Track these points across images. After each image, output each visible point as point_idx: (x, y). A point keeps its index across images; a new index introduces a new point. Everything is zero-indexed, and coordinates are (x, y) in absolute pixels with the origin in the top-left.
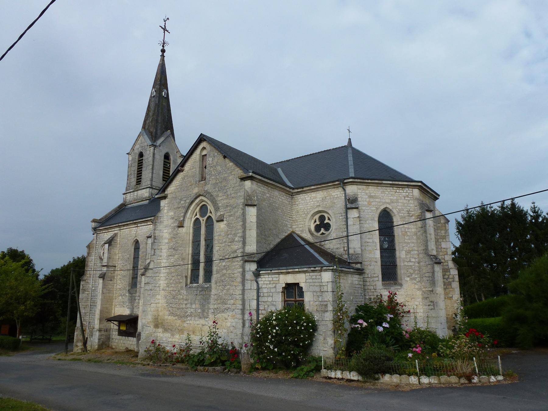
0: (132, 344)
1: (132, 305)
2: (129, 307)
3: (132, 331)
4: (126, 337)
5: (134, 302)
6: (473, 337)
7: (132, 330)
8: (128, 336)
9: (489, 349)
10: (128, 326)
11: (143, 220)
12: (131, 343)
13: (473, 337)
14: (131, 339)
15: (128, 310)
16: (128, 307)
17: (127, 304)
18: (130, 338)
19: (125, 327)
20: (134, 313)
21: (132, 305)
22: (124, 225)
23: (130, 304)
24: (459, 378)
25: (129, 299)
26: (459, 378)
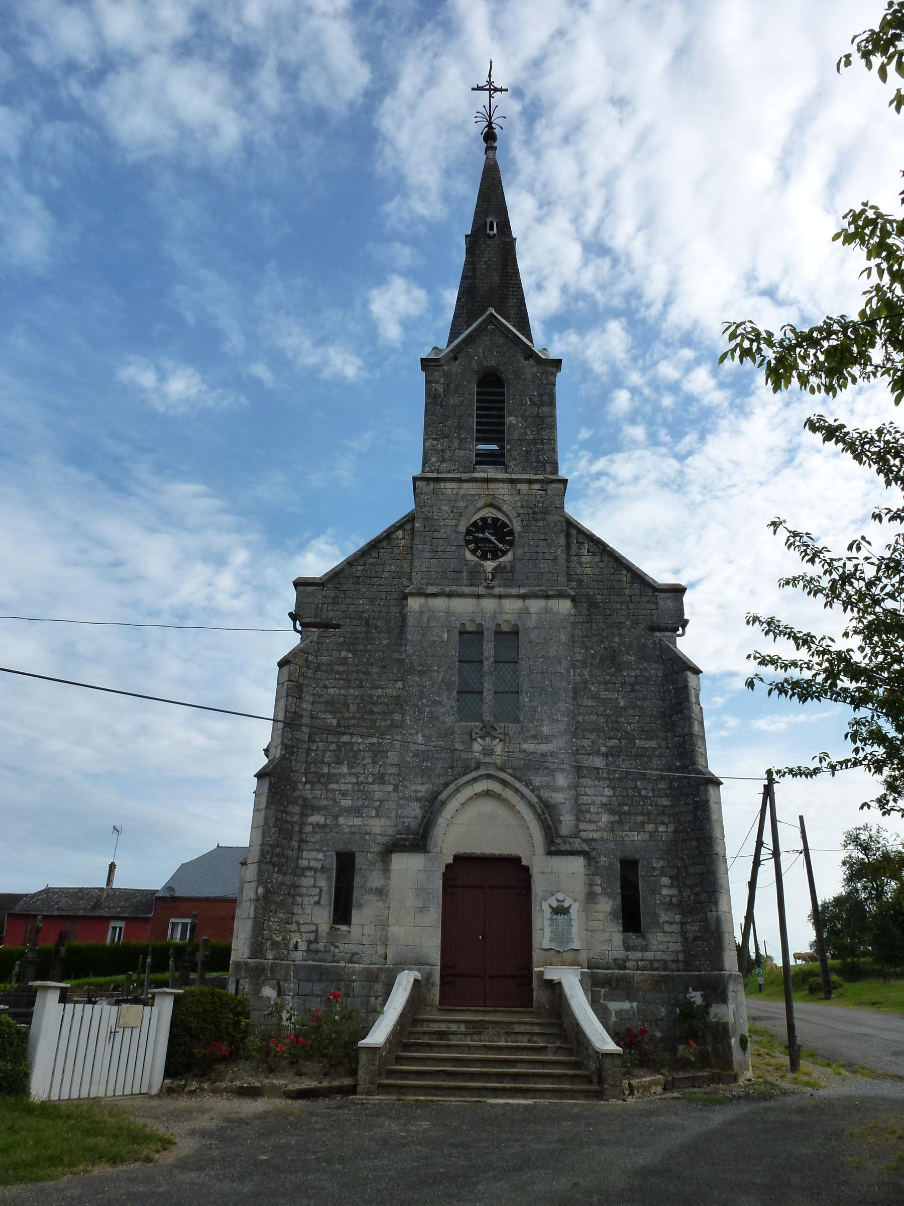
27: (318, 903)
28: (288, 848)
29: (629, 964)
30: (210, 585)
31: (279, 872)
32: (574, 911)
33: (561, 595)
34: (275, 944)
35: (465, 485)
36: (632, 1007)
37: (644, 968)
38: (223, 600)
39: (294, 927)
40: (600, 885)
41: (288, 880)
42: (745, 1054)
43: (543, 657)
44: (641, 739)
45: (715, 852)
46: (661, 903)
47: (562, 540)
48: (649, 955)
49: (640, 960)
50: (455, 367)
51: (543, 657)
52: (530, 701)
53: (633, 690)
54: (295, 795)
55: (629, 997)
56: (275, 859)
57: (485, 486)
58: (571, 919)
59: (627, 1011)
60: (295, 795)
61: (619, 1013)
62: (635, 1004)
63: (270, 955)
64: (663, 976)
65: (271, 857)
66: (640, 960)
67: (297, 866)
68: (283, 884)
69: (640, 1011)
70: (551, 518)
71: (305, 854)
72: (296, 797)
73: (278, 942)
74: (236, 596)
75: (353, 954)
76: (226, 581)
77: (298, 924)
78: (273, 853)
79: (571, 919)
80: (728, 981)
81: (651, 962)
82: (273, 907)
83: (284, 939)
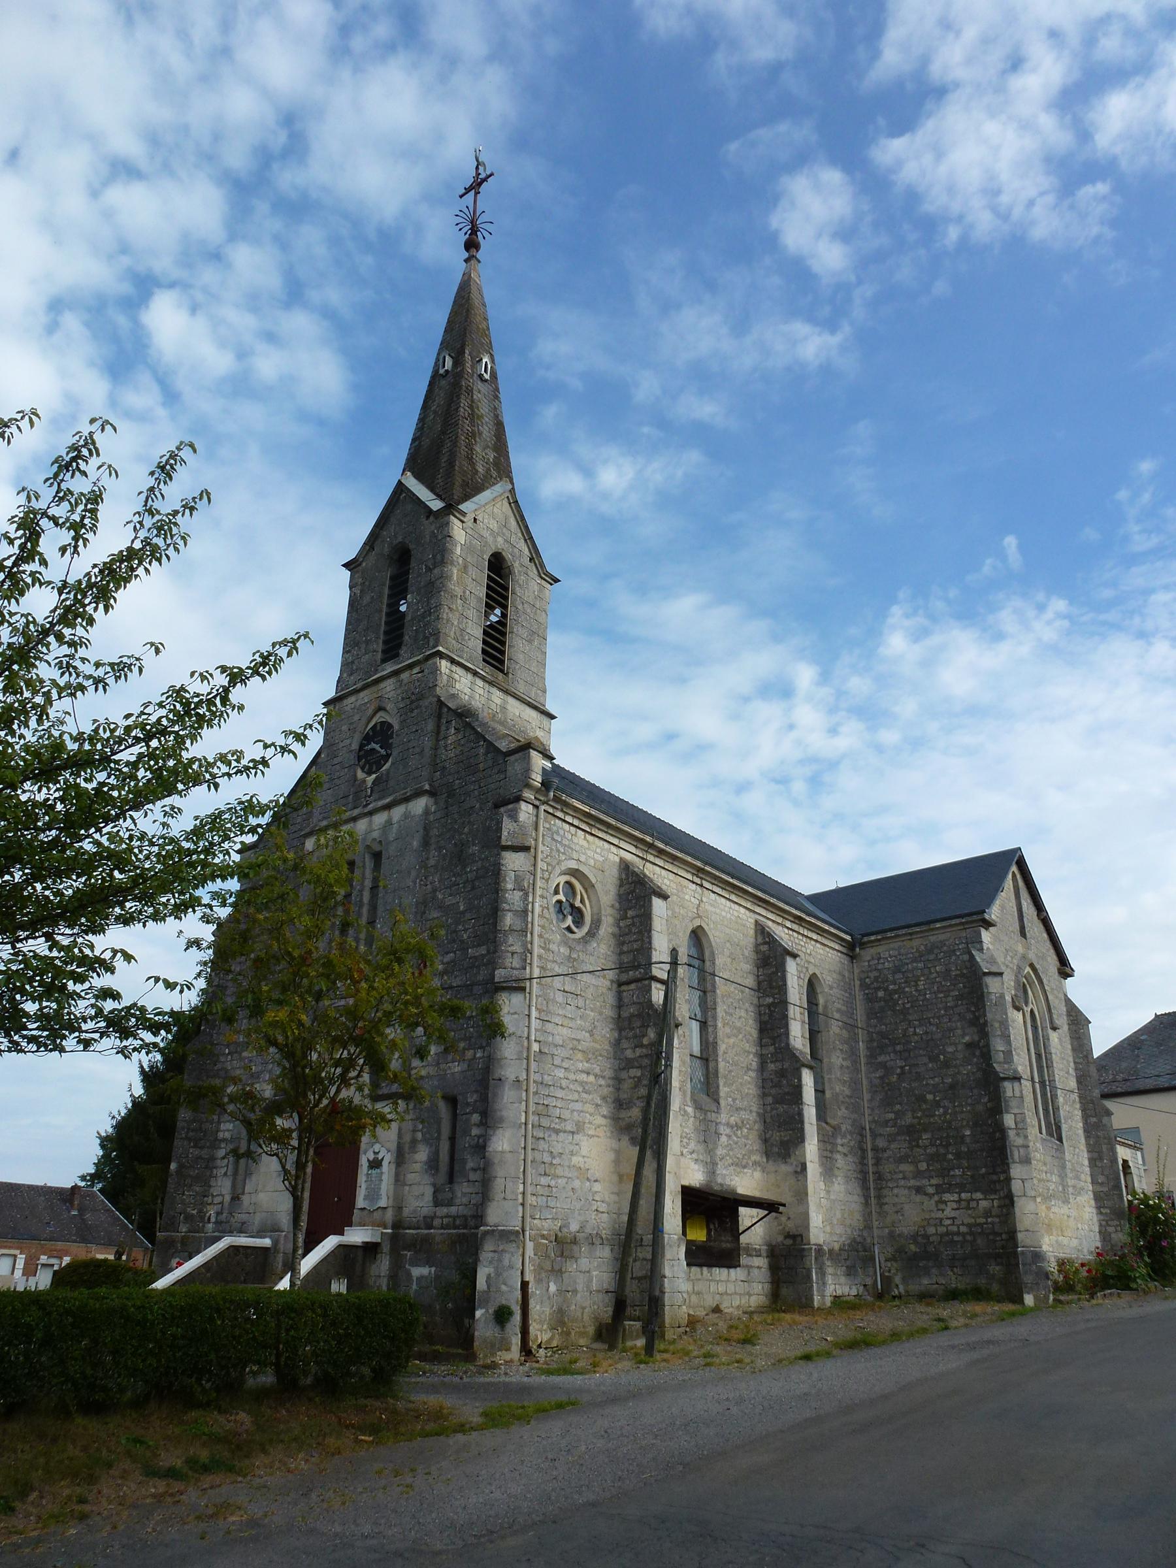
0: (726, 1293)
1: (710, 1152)
2: (701, 1157)
3: (729, 1245)
4: (705, 1269)
5: (715, 1143)
6: (944, 1107)
7: (727, 1242)
8: (710, 1265)
9: (930, 1065)
10: (712, 1226)
11: (760, 894)
12: (721, 1289)
13: (944, 1107)
14: (720, 1273)
15: (696, 1167)
16: (694, 1156)
17: (692, 1145)
18: (716, 1271)
19: (705, 1232)
20: (719, 1180)
21: (710, 1152)
22: (661, 853)
23: (701, 1148)
24: (491, 58)
25: (696, 1129)
26: (491, 58)
27: (225, 1174)
28: (207, 1122)
29: (437, 1222)
30: (791, 727)
31: (195, 1146)
32: (385, 1163)
33: (418, 794)
34: (189, 1218)
35: (362, 694)
36: (430, 1273)
37: (447, 1227)
38: (820, 743)
39: (209, 1200)
40: (421, 1131)
41: (205, 1153)
42: (503, 1330)
43: (397, 872)
44: (473, 947)
45: (496, 1076)
46: (470, 1146)
47: (430, 726)
48: (453, 1210)
49: (446, 1217)
50: (372, 557)
51: (397, 872)
52: (381, 928)
53: (473, 888)
54: (216, 1068)
55: (429, 1263)
56: (191, 1134)
57: (374, 689)
58: (382, 1173)
59: (426, 1277)
60: (216, 1068)
61: (420, 1279)
62: (433, 1269)
63: (184, 1228)
64: (459, 1235)
65: (187, 1132)
66: (446, 1217)
67: (216, 1139)
68: (200, 1157)
69: (437, 1277)
70: (426, 703)
71: (222, 1127)
72: (218, 1070)
73: (193, 1215)
74: (833, 731)
75: (243, 1223)
76: (808, 716)
77: (213, 1196)
78: (188, 1129)
79: (382, 1173)
80: (481, 1238)
81: (454, 1218)
82: (188, 1181)
83: (200, 1211)
